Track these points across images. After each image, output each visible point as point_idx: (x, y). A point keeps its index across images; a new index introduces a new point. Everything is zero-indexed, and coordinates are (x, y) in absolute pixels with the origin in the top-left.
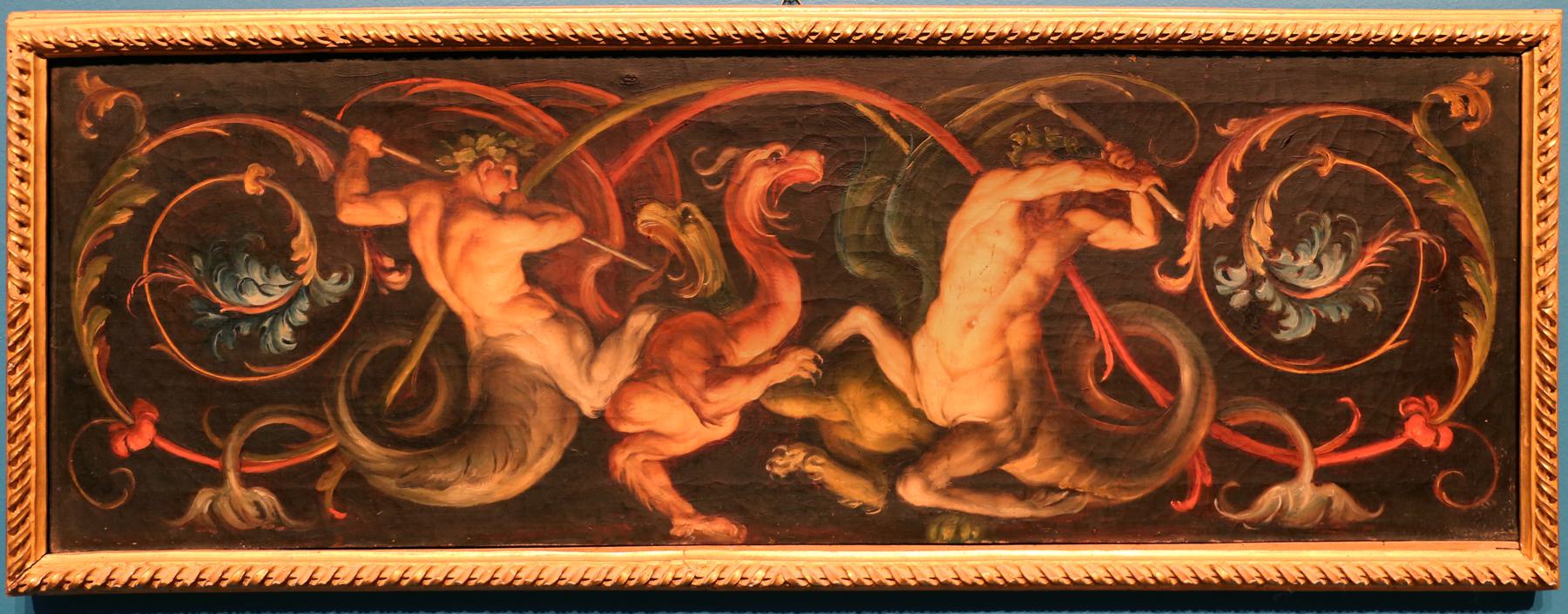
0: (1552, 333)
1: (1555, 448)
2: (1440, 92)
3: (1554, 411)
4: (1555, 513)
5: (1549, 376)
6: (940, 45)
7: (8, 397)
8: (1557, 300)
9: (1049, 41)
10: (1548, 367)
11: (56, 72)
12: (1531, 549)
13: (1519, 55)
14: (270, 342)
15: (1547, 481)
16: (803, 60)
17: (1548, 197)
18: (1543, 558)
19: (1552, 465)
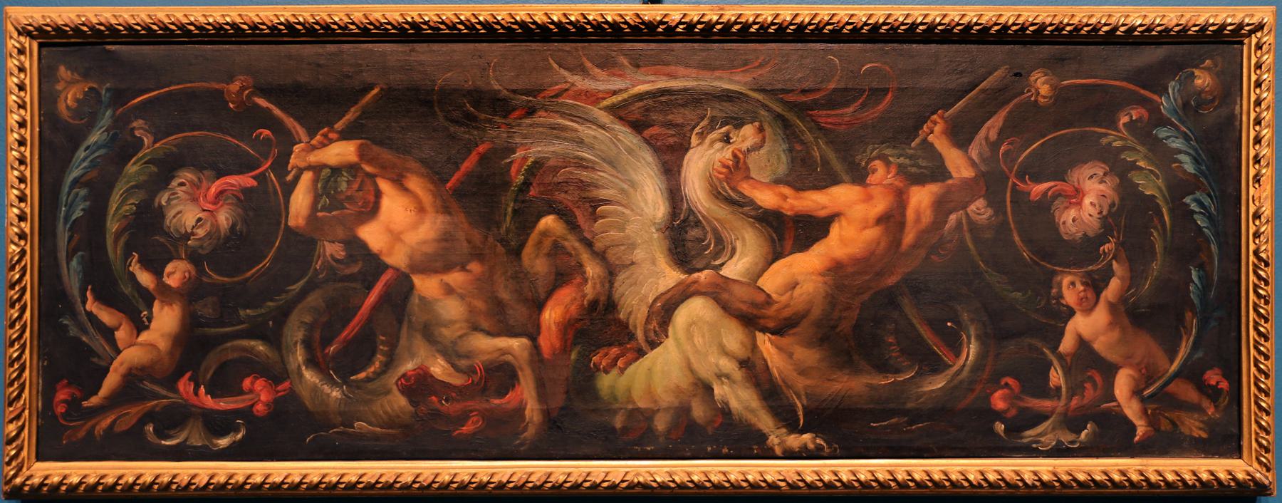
0: (1267, 404)
1: (1268, 424)
2: (1194, 70)
3: (1269, 320)
4: (1268, 350)
5: (1265, 457)
6: (844, 33)
7: (8, 330)
8: (1271, 129)
9: (936, 30)
10: (1262, 283)
11: (45, 51)
12: (1252, 460)
13: (1242, 43)
14: (1042, 100)
15: (1263, 343)
16: (1128, 47)
17: (1262, 236)
18: (1260, 463)
19: (1266, 291)
